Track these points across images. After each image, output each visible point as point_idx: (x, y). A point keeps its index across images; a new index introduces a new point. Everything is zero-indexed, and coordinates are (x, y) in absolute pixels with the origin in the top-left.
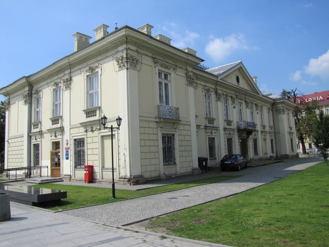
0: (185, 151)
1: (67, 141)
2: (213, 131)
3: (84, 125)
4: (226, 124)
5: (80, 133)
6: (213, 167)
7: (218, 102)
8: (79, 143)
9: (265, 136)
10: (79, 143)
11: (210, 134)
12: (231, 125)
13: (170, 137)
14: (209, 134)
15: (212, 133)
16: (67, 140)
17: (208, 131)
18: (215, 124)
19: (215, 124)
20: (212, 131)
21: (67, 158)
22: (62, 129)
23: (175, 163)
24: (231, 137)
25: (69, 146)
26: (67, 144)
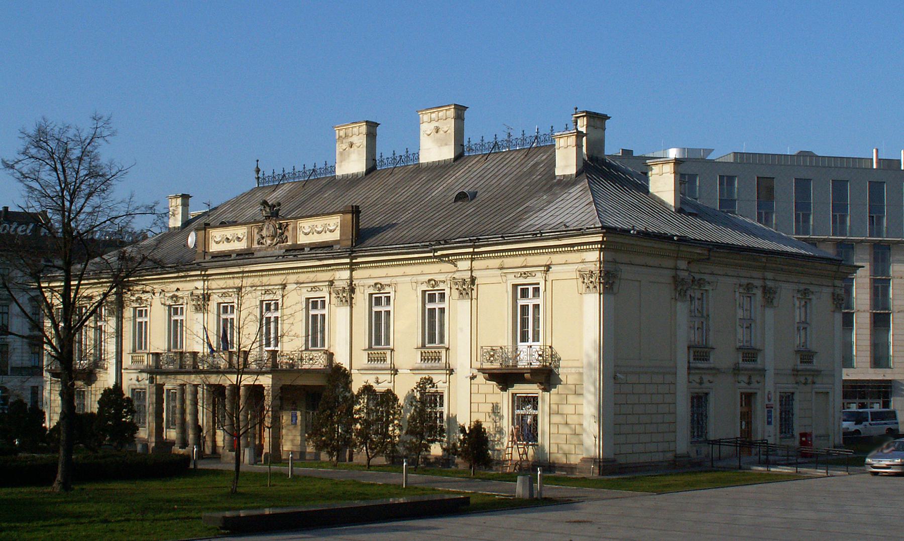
0: (663, 423)
1: (769, 393)
2: (706, 378)
3: (796, 372)
4: (799, 360)
5: (788, 385)
6: (472, 501)
7: (679, 304)
8: (787, 400)
9: (749, 383)
10: (787, 400)
11: (698, 385)
12: (811, 362)
13: (701, 397)
14: (743, 384)
15: (701, 383)
16: (770, 389)
17: (740, 378)
18: (759, 364)
19: (759, 364)
20: (701, 379)
21: (769, 423)
22: (762, 372)
23: (793, 435)
24: (705, 391)
25: (772, 402)
26: (769, 400)
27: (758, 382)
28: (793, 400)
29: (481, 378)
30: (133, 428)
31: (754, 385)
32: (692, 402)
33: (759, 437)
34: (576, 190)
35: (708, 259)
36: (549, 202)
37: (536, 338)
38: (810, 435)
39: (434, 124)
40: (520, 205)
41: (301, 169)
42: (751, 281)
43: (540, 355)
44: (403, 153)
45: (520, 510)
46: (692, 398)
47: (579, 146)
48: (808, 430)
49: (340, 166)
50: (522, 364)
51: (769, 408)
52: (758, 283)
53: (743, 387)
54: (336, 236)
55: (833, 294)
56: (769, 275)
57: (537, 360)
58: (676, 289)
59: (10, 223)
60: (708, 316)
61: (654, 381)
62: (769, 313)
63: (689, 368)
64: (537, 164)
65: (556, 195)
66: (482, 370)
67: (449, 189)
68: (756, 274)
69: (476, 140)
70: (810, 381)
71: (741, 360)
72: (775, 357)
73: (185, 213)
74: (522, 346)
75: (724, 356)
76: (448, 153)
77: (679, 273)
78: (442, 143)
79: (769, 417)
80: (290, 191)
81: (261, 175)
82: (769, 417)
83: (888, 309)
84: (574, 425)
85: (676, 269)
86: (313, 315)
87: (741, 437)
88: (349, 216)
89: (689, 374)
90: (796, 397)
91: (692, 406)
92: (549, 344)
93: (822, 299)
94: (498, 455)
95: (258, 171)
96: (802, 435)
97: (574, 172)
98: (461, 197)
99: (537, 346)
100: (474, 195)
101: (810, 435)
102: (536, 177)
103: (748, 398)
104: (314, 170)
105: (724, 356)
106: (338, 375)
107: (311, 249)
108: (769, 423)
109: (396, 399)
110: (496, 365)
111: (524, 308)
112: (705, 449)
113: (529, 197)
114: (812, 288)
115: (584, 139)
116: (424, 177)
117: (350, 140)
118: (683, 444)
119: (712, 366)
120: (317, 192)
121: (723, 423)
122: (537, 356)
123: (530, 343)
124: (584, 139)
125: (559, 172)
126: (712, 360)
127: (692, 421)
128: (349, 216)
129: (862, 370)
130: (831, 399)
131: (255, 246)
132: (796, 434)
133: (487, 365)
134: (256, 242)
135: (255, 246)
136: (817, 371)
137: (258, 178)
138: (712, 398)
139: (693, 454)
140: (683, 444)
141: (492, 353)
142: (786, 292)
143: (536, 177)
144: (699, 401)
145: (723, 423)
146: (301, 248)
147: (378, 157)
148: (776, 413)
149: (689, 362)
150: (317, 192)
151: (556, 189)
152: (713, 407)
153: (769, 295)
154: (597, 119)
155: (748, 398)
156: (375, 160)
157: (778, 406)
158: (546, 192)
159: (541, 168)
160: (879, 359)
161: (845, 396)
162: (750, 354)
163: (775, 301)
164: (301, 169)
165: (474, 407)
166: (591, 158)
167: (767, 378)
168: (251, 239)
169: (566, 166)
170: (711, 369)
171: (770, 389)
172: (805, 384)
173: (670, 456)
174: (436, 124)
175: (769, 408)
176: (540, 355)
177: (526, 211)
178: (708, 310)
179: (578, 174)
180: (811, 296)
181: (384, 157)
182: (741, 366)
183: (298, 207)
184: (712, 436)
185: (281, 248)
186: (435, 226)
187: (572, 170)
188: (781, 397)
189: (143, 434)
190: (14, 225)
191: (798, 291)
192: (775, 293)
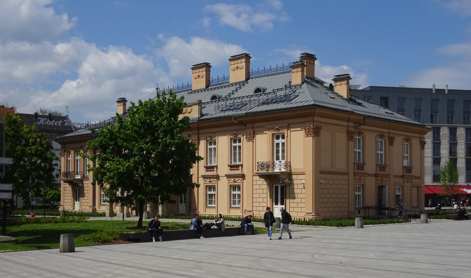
12: (410, 172)
15: (360, 180)
19: (387, 172)
29: (258, 178)
41: (182, 85)
47: (303, 71)
59: (52, 120)
63: (354, 173)
72: (396, 169)
75: (370, 168)
86: (210, 149)
89: (354, 176)
92: (289, 160)
93: (416, 143)
94: (63, 123)
100: (264, 90)
103: (380, 189)
105: (370, 168)
111: (278, 145)
122: (283, 166)
133: (260, 171)
141: (262, 166)
142: (398, 141)
153: (391, 141)
155: (380, 189)
162: (382, 168)
165: (254, 191)
190: (54, 121)
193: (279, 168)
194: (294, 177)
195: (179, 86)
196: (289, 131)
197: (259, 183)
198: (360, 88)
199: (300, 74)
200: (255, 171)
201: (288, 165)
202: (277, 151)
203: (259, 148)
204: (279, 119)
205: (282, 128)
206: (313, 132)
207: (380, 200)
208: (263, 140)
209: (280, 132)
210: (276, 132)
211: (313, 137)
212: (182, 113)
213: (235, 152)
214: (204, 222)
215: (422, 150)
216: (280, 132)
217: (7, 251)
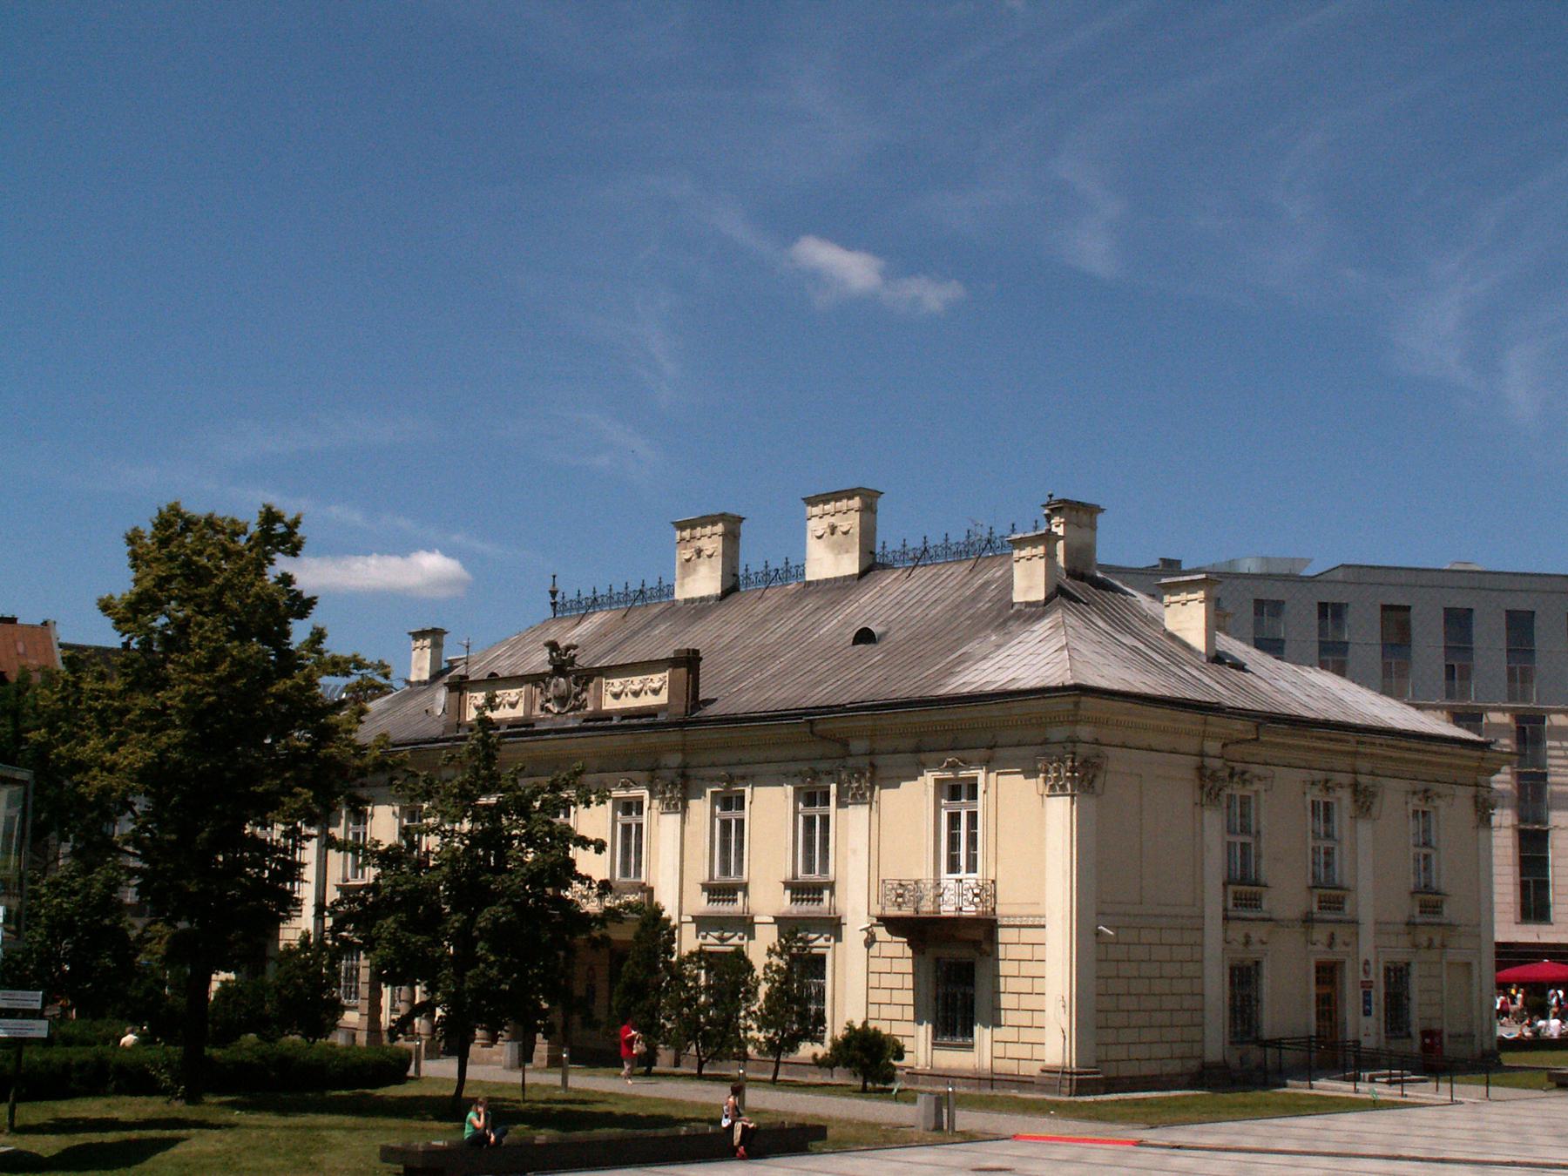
1: (1367, 963)
7: (1207, 814)
8: (1397, 976)
10: (1397, 976)
12: (1439, 913)
21: (1367, 1013)
23: (1409, 1035)
24: (1255, 956)
26: (1366, 972)
27: (1346, 944)
28: (1408, 974)
29: (881, 933)
30: (338, 1009)
31: (1339, 948)
32: (1232, 976)
33: (1350, 1036)
34: (1042, 627)
35: (1257, 739)
36: (999, 646)
37: (972, 867)
38: (1440, 1032)
39: (828, 520)
40: (952, 651)
41: (622, 590)
42: (1330, 775)
43: (976, 895)
44: (781, 565)
45: (603, 1070)
46: (1232, 969)
47: (1050, 556)
48: (1436, 1026)
49: (682, 585)
50: (948, 910)
51: (1367, 987)
52: (1345, 779)
53: (1320, 953)
54: (663, 698)
55: (1476, 797)
56: (1364, 765)
57: (972, 903)
58: (1202, 787)
60: (1258, 832)
61: (1144, 940)
62: (1365, 829)
64: (987, 584)
65: (1010, 636)
66: (885, 921)
67: (846, 623)
68: (1342, 762)
69: (894, 545)
70: (1437, 942)
71: (1315, 909)
73: (435, 660)
74: (947, 879)
76: (850, 565)
77: (1207, 761)
78: (839, 549)
79: (1367, 1002)
80: (602, 624)
81: (558, 599)
82: (1367, 1002)
83: (1546, 823)
84: (1041, 1010)
85: (1202, 754)
87: (1318, 1036)
88: (683, 670)
90: (1415, 971)
91: (1232, 982)
95: (554, 594)
96: (1426, 1033)
97: (1041, 596)
98: (865, 636)
99: (970, 879)
101: (1440, 1032)
102: (983, 605)
103: (1328, 973)
104: (641, 592)
106: (653, 923)
107: (624, 718)
108: (1367, 1013)
109: (750, 968)
110: (907, 911)
112: (1255, 1054)
113: (960, 642)
114: (1436, 787)
115: (1060, 544)
116: (810, 603)
117: (699, 544)
118: (1215, 1044)
119: (1266, 916)
120: (645, 627)
121: (1286, 1006)
122: (970, 896)
123: (962, 874)
124: (1060, 544)
125: (1018, 597)
126: (1264, 907)
127: (1233, 1009)
128: (683, 670)
129: (1509, 929)
130: (1475, 973)
131: (537, 712)
132: (1415, 1030)
133: (892, 911)
134: (538, 707)
135: (537, 712)
136: (1450, 925)
137: (554, 604)
138: (1266, 970)
139: (1234, 1061)
140: (1215, 1044)
141: (902, 890)
142: (1394, 798)
143: (983, 605)
144: (1244, 978)
145: (1286, 1006)
146: (608, 716)
147: (741, 572)
148: (1379, 994)
149: (1225, 910)
150: (645, 627)
151: (1013, 626)
152: (1268, 985)
153: (1364, 800)
154: (1080, 513)
155: (1328, 973)
156: (735, 575)
157: (1382, 984)
158: (996, 629)
159: (992, 591)
160: (1535, 905)
161: (1500, 966)
163: (1374, 810)
164: (622, 590)
166: (1073, 573)
167: (1361, 937)
168: (530, 703)
169: (1029, 589)
170: (1264, 920)
171: (1368, 953)
172: (1430, 946)
173: (1193, 1065)
174: (833, 520)
175: (1367, 987)
176: (976, 895)
177: (961, 660)
178: (1258, 823)
179: (1048, 599)
180: (1438, 802)
181: (751, 571)
182: (1418, 920)
183: (613, 649)
184: (1267, 1033)
185: (576, 717)
186: (820, 683)
187: (1039, 595)
188: (1387, 970)
189: (351, 1018)
191: (1414, 793)
192: (1374, 795)
193: (955, 898)
194: (1004, 935)
195: (614, 591)
196: (992, 775)
197: (888, 950)
198: (1309, 571)
199: (1040, 566)
200: (876, 910)
201: (988, 891)
202: (959, 842)
203: (886, 842)
204: (957, 737)
205: (968, 764)
206: (1072, 779)
207: (1328, 1006)
208: (911, 804)
209: (963, 774)
210: (949, 775)
211: (1072, 796)
212: (652, 797)
213: (814, 838)
214: (135, 980)
215: (1483, 834)
216: (963, 774)
217: (559, 1107)
